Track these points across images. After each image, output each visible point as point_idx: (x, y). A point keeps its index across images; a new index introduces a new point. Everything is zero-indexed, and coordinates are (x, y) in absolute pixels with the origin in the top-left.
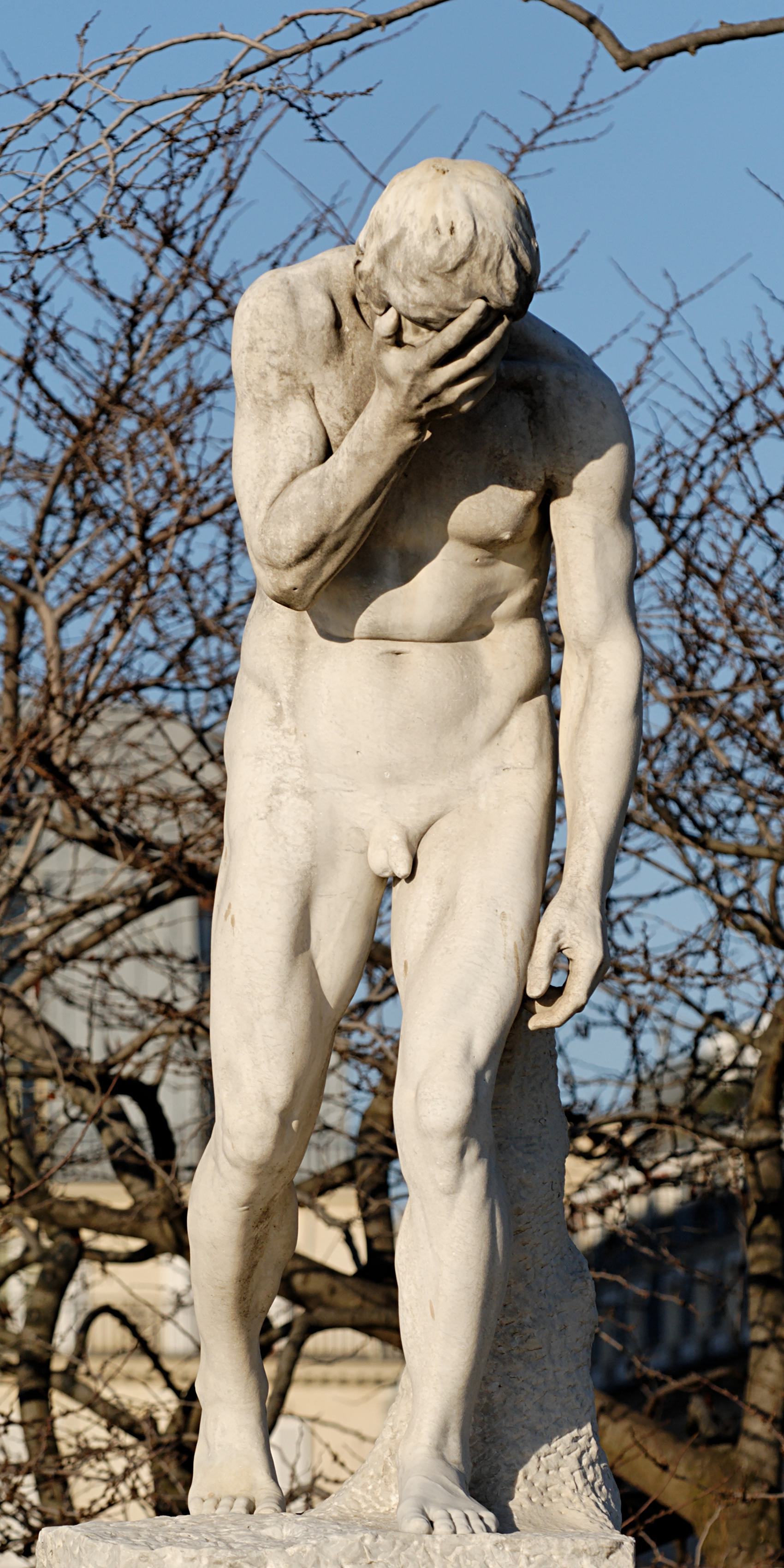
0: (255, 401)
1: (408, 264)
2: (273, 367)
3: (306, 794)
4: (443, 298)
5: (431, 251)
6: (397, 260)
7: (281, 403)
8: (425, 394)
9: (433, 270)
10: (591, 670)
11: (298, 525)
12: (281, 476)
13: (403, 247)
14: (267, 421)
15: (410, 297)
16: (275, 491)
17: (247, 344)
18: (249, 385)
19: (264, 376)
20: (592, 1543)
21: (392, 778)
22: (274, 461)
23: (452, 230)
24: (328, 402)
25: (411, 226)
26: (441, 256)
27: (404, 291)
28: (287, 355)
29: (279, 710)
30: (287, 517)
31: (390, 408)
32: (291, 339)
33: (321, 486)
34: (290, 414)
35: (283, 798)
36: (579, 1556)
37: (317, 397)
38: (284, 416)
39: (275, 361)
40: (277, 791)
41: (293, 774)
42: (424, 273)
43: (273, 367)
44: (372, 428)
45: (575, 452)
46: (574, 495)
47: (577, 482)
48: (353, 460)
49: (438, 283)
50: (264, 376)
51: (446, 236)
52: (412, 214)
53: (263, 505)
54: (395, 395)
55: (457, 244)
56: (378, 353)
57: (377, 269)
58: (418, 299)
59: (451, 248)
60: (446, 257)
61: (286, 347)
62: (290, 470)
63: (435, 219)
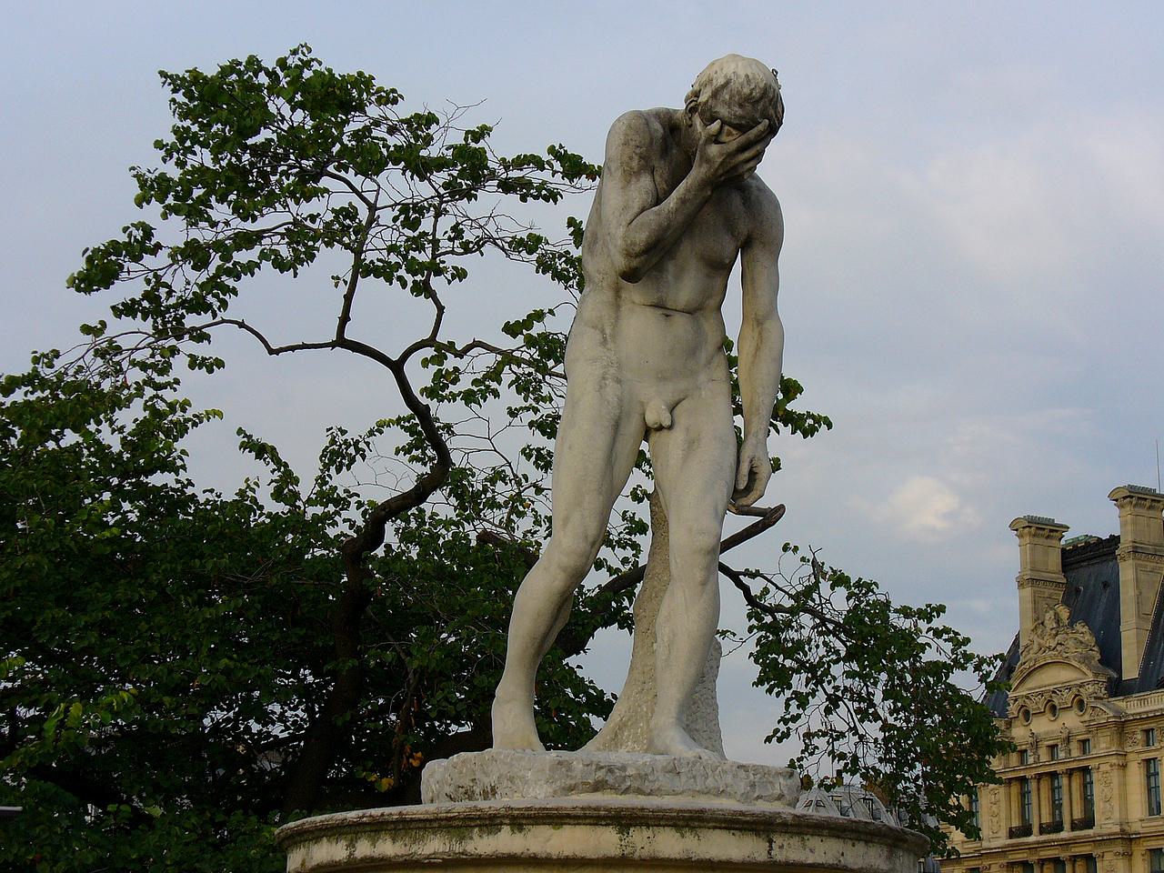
3: (619, 381)
7: (637, 174)
10: (760, 334)
12: (636, 210)
20: (1092, 582)
21: (662, 377)
24: (661, 177)
26: (751, 93)
29: (605, 339)
31: (704, 177)
32: (647, 141)
35: (607, 382)
36: (778, 776)
39: (638, 151)
40: (604, 378)
41: (612, 371)
43: (636, 154)
49: (749, 107)
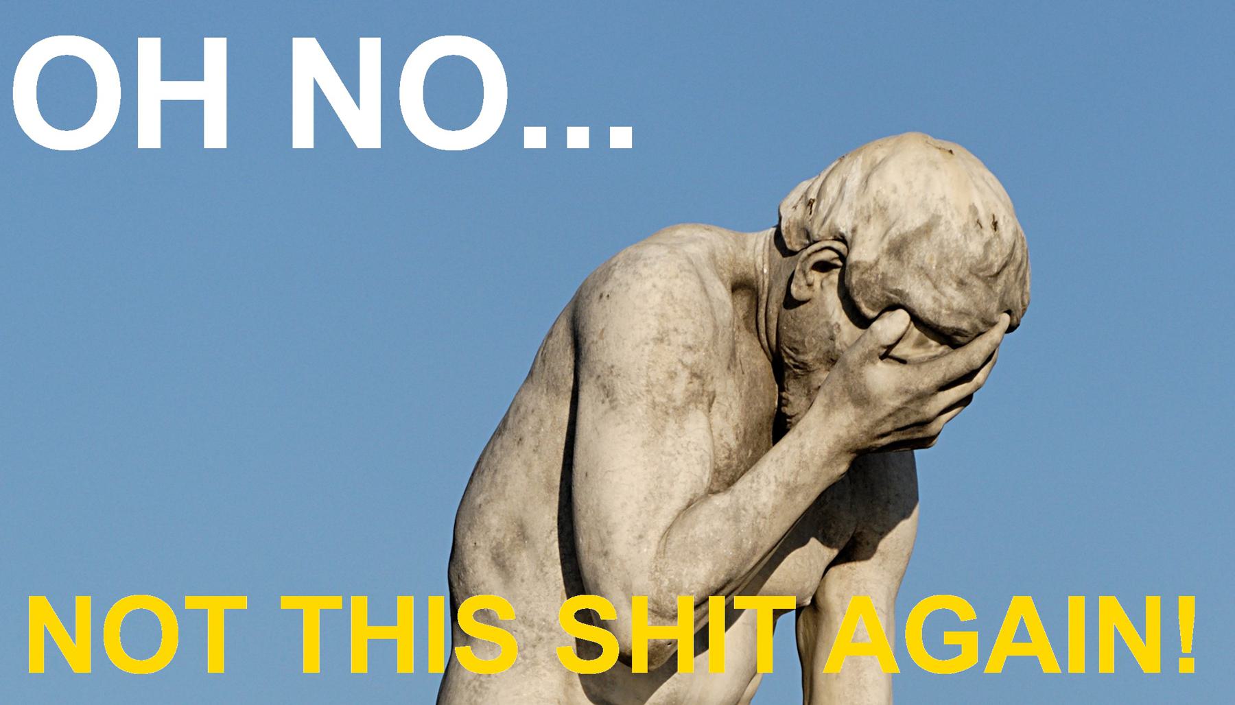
0: (654, 405)
1: (945, 259)
2: (685, 366)
4: (983, 307)
5: (975, 248)
6: (925, 252)
7: (681, 412)
8: (914, 418)
9: (974, 271)
11: (709, 565)
12: (678, 503)
13: (935, 240)
14: (660, 431)
15: (944, 301)
16: (669, 520)
17: (654, 333)
18: (650, 384)
19: (672, 376)
22: (672, 483)
23: (995, 224)
25: (946, 214)
26: (986, 256)
27: (935, 293)
28: (702, 353)
30: (695, 554)
32: (709, 334)
33: (736, 519)
34: (689, 426)
37: (715, 404)
38: (681, 428)
42: (963, 273)
43: (685, 366)
44: (813, 455)
45: (891, 507)
46: (876, 559)
47: (883, 545)
48: (783, 491)
49: (978, 286)
50: (672, 376)
51: (988, 232)
52: (943, 199)
53: (654, 536)
54: (859, 419)
55: (1002, 242)
56: (862, 365)
57: (884, 262)
58: (955, 304)
59: (996, 247)
60: (992, 257)
61: (702, 343)
62: (689, 496)
63: (974, 210)
